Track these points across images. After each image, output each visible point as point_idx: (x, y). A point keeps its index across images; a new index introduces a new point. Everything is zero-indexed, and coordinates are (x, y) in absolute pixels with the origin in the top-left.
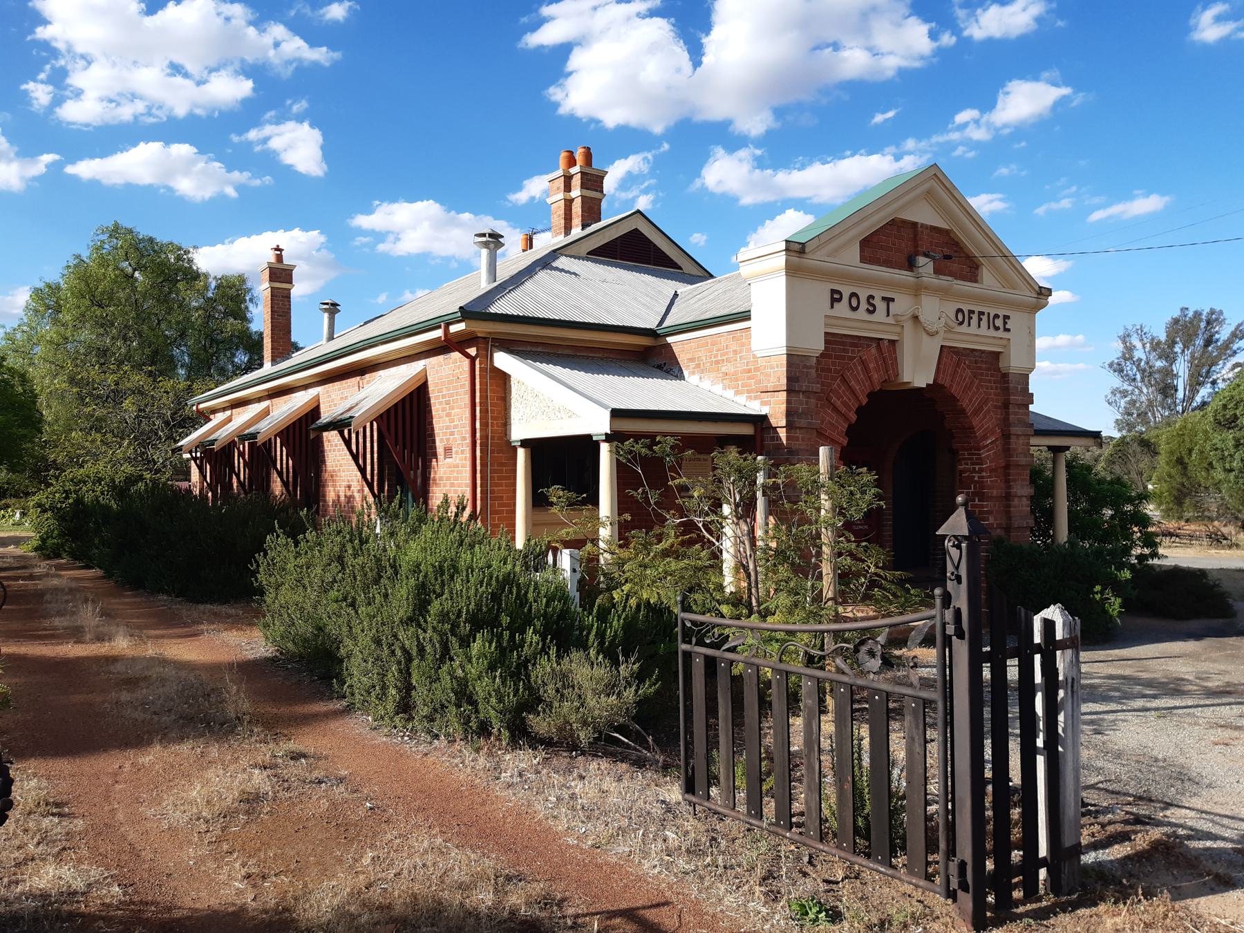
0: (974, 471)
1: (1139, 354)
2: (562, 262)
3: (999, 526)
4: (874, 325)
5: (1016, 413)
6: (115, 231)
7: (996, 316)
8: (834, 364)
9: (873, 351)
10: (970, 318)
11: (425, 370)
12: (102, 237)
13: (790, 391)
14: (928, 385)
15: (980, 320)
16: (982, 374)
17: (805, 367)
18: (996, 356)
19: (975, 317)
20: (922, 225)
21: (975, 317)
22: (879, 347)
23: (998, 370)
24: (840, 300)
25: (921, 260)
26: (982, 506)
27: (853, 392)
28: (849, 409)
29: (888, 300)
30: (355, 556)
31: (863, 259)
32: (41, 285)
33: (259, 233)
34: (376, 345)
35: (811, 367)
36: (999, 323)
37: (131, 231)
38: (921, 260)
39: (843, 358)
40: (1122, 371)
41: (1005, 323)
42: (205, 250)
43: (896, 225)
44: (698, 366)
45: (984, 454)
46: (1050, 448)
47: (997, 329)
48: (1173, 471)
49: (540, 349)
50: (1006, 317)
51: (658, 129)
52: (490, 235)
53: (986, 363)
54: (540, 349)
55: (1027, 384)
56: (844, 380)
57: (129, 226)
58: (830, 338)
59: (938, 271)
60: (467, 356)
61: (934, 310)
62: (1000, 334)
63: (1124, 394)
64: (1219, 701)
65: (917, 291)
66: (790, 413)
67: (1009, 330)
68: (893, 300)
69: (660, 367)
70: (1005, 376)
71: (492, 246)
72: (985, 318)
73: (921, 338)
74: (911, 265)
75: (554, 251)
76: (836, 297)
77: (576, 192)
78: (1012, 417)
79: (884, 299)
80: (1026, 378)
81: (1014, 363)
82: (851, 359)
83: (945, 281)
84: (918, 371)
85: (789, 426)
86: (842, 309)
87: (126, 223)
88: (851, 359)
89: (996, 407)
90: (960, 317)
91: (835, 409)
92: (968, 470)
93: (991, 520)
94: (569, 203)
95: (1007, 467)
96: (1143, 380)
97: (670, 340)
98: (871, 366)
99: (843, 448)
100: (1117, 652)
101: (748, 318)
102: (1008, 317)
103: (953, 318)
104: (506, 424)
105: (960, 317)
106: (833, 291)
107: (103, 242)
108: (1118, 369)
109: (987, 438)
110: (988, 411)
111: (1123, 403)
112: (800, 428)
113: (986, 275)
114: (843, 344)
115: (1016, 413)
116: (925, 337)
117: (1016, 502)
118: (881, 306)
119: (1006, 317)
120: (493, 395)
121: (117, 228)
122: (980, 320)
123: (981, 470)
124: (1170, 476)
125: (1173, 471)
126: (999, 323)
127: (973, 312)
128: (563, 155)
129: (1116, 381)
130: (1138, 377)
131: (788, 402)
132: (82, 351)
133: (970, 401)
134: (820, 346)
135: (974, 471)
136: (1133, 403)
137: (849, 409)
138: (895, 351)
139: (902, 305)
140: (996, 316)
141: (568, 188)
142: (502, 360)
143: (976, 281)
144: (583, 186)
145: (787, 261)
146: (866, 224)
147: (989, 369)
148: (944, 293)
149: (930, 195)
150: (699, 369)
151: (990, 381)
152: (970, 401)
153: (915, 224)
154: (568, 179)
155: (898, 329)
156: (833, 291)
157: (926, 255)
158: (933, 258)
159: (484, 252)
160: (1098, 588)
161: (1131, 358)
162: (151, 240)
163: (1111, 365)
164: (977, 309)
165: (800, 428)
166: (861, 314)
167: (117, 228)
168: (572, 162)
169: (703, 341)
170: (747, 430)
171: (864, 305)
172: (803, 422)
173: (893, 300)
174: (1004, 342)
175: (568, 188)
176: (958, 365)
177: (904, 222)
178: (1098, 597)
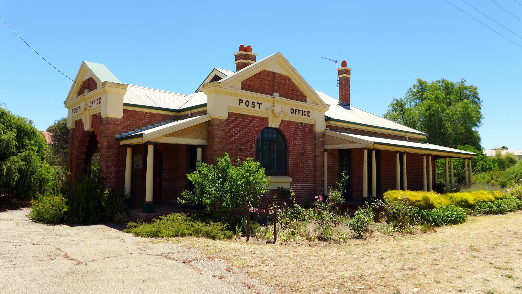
7: (305, 111)
15: (299, 112)
19: (297, 111)
21: (297, 111)
24: (242, 103)
29: (260, 104)
30: (264, 183)
36: (306, 113)
51: (421, 200)
58: (230, 114)
62: (307, 117)
72: (301, 112)
79: (258, 103)
86: (243, 105)
90: (292, 111)
105: (292, 111)
106: (240, 100)
118: (257, 106)
119: (308, 112)
122: (299, 112)
126: (306, 113)
134: (225, 116)
140: (305, 111)
146: (309, 91)
153: (273, 72)
156: (240, 100)
164: (298, 109)
171: (251, 105)
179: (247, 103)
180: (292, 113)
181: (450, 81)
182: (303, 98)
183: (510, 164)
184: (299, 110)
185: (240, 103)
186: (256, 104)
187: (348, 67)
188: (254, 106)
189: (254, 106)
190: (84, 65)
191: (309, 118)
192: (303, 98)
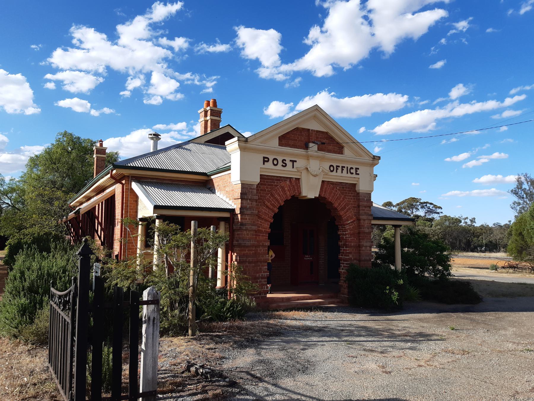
0: (343, 235)
1: (526, 186)
2: (190, 146)
3: (355, 259)
4: (288, 172)
5: (364, 210)
6: (65, 134)
7: (352, 168)
8: (267, 188)
9: (288, 182)
10: (337, 169)
11: (115, 189)
12: (60, 137)
13: (242, 198)
14: (315, 197)
15: (342, 170)
16: (346, 193)
17: (251, 189)
18: (354, 185)
19: (340, 169)
20: (312, 130)
21: (340, 169)
22: (290, 181)
23: (356, 191)
24: (268, 161)
25: (311, 145)
26: (346, 250)
27: (277, 200)
28: (274, 206)
29: (293, 162)
31: (280, 144)
32: (33, 156)
33: (129, 134)
34: (99, 180)
35: (254, 189)
36: (353, 171)
37: (71, 134)
38: (311, 145)
39: (272, 185)
40: (517, 194)
41: (356, 171)
42: (108, 140)
43: (298, 131)
44: (220, 188)
45: (347, 227)
46: (393, 226)
47: (352, 173)
48: (518, 238)
49: (155, 181)
50: (357, 169)
52: (154, 135)
53: (348, 188)
54: (155, 181)
55: (370, 197)
56: (272, 195)
57: (70, 132)
59: (319, 149)
60: (122, 183)
61: (315, 165)
62: (354, 175)
63: (519, 204)
64: (373, 339)
65: (308, 158)
66: (241, 209)
67: (358, 174)
68: (296, 161)
69: (209, 189)
70: (358, 193)
71: (155, 139)
72: (345, 169)
73: (311, 176)
74: (306, 147)
75: (189, 141)
76: (265, 160)
77: (208, 118)
78: (361, 212)
79: (291, 161)
80: (369, 195)
81: (362, 188)
82: (276, 186)
83: (321, 153)
84: (310, 190)
85: (241, 213)
86: (269, 165)
87: (70, 131)
88: (276, 186)
89: (354, 207)
91: (267, 207)
92: (342, 234)
93: (351, 256)
94: (206, 122)
95: (359, 233)
96: (527, 197)
97: (212, 177)
98: (286, 189)
99: (271, 223)
100: (394, 316)
101: (230, 170)
102: (358, 169)
103: (328, 170)
104: (136, 212)
106: (264, 158)
107: (60, 138)
108: (515, 192)
109: (348, 220)
110: (349, 209)
111: (518, 208)
112: (248, 215)
113: (346, 151)
114: (273, 179)
115: (364, 210)
116: (311, 177)
117: (364, 248)
118: (289, 164)
119: (356, 169)
120: (132, 200)
121: (66, 132)
122: (342, 170)
123: (346, 235)
124: (516, 240)
125: (518, 238)
126: (353, 171)
127: (339, 166)
128: (206, 102)
129: (515, 199)
130: (525, 196)
131: (241, 203)
132: (45, 182)
133: (340, 204)
134: (258, 180)
135: (343, 235)
136: (523, 208)
137: (274, 206)
138: (299, 183)
139: (300, 163)
140: (352, 168)
141: (206, 116)
142: (135, 186)
143: (342, 153)
144: (211, 115)
145: (239, 145)
147: (350, 191)
148: (322, 159)
149: (315, 117)
150: (220, 190)
151: (351, 196)
152: (340, 204)
153: (309, 130)
154: (206, 112)
155: (299, 174)
156: (264, 158)
157: (313, 143)
158: (317, 144)
159: (152, 141)
160: (388, 287)
161: (521, 188)
162: (79, 138)
163: (512, 191)
165: (248, 215)
166: (279, 167)
167: (66, 132)
168: (208, 105)
169: (223, 177)
170: (227, 215)
171: (280, 163)
172: (249, 212)
173: (296, 161)
174: (357, 179)
175: (206, 116)
176: (333, 189)
177: (303, 129)
178: (387, 292)
179: (275, 162)
180: (332, 171)
181: (452, 216)
182: (339, 148)
183: (56, 312)
184: (343, 167)
185: (264, 162)
186: (288, 162)
187: (219, 106)
188: (285, 165)
189: (285, 165)
190: (151, 72)
191: (357, 176)
192: (339, 148)
